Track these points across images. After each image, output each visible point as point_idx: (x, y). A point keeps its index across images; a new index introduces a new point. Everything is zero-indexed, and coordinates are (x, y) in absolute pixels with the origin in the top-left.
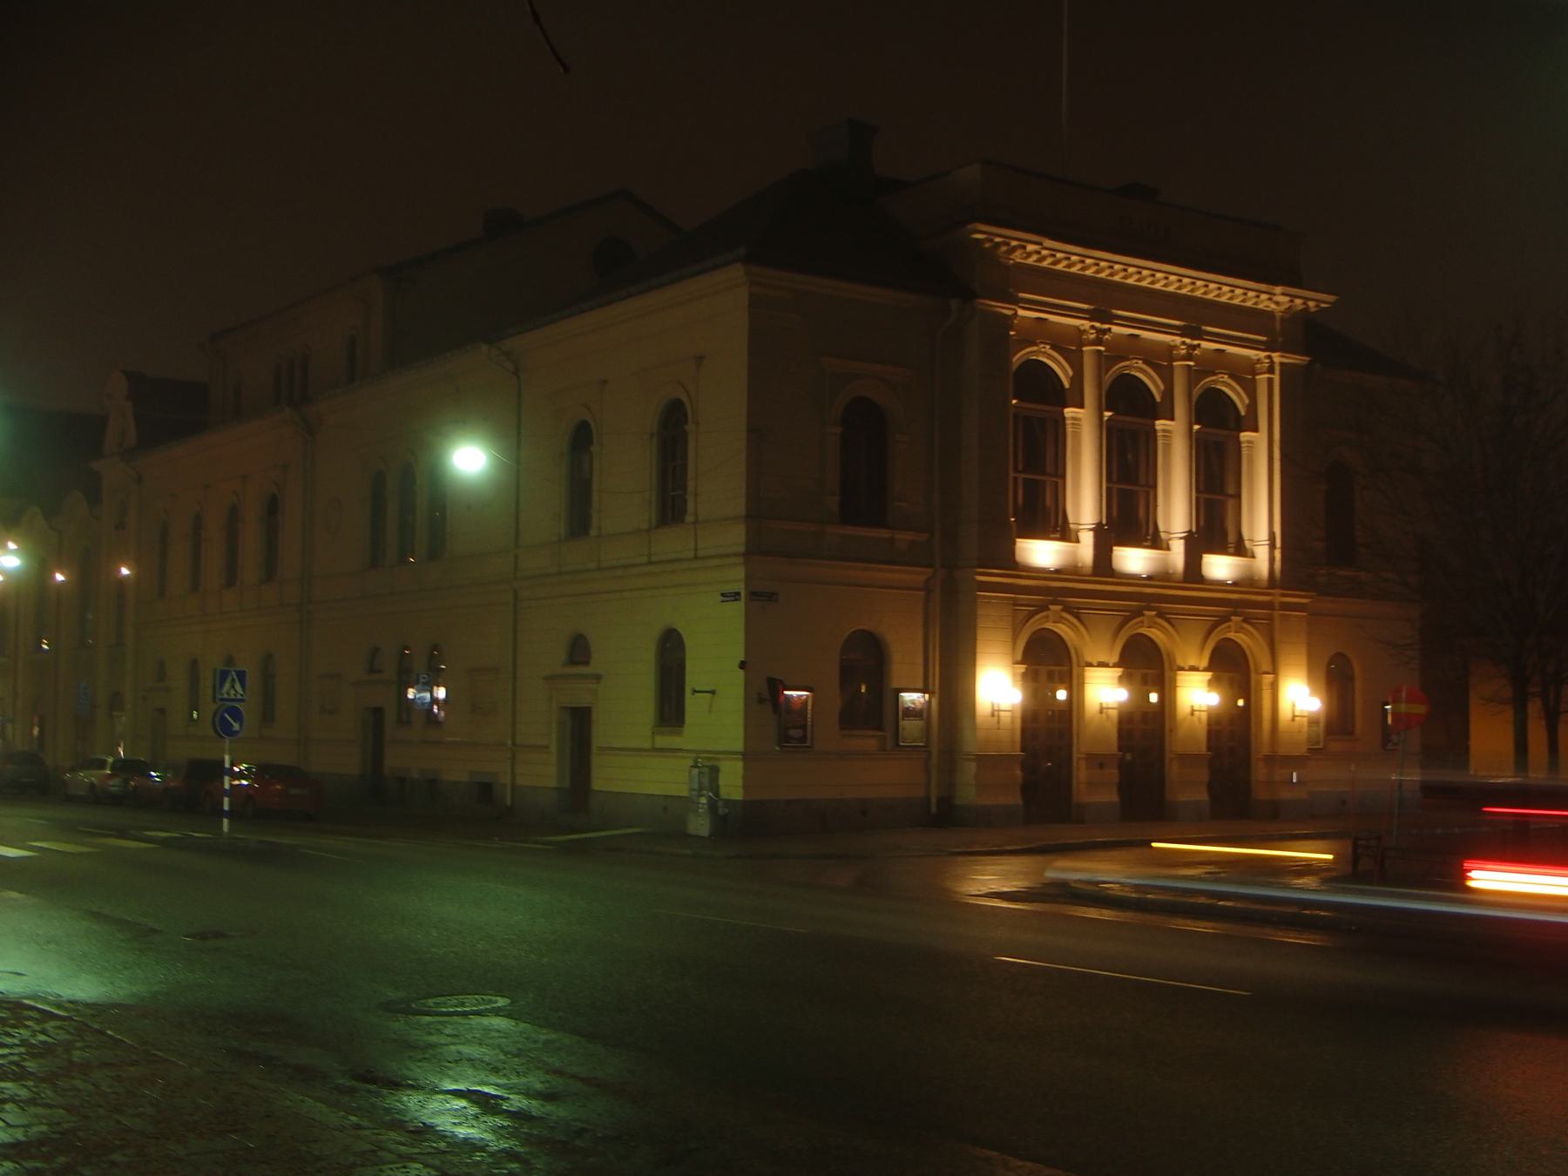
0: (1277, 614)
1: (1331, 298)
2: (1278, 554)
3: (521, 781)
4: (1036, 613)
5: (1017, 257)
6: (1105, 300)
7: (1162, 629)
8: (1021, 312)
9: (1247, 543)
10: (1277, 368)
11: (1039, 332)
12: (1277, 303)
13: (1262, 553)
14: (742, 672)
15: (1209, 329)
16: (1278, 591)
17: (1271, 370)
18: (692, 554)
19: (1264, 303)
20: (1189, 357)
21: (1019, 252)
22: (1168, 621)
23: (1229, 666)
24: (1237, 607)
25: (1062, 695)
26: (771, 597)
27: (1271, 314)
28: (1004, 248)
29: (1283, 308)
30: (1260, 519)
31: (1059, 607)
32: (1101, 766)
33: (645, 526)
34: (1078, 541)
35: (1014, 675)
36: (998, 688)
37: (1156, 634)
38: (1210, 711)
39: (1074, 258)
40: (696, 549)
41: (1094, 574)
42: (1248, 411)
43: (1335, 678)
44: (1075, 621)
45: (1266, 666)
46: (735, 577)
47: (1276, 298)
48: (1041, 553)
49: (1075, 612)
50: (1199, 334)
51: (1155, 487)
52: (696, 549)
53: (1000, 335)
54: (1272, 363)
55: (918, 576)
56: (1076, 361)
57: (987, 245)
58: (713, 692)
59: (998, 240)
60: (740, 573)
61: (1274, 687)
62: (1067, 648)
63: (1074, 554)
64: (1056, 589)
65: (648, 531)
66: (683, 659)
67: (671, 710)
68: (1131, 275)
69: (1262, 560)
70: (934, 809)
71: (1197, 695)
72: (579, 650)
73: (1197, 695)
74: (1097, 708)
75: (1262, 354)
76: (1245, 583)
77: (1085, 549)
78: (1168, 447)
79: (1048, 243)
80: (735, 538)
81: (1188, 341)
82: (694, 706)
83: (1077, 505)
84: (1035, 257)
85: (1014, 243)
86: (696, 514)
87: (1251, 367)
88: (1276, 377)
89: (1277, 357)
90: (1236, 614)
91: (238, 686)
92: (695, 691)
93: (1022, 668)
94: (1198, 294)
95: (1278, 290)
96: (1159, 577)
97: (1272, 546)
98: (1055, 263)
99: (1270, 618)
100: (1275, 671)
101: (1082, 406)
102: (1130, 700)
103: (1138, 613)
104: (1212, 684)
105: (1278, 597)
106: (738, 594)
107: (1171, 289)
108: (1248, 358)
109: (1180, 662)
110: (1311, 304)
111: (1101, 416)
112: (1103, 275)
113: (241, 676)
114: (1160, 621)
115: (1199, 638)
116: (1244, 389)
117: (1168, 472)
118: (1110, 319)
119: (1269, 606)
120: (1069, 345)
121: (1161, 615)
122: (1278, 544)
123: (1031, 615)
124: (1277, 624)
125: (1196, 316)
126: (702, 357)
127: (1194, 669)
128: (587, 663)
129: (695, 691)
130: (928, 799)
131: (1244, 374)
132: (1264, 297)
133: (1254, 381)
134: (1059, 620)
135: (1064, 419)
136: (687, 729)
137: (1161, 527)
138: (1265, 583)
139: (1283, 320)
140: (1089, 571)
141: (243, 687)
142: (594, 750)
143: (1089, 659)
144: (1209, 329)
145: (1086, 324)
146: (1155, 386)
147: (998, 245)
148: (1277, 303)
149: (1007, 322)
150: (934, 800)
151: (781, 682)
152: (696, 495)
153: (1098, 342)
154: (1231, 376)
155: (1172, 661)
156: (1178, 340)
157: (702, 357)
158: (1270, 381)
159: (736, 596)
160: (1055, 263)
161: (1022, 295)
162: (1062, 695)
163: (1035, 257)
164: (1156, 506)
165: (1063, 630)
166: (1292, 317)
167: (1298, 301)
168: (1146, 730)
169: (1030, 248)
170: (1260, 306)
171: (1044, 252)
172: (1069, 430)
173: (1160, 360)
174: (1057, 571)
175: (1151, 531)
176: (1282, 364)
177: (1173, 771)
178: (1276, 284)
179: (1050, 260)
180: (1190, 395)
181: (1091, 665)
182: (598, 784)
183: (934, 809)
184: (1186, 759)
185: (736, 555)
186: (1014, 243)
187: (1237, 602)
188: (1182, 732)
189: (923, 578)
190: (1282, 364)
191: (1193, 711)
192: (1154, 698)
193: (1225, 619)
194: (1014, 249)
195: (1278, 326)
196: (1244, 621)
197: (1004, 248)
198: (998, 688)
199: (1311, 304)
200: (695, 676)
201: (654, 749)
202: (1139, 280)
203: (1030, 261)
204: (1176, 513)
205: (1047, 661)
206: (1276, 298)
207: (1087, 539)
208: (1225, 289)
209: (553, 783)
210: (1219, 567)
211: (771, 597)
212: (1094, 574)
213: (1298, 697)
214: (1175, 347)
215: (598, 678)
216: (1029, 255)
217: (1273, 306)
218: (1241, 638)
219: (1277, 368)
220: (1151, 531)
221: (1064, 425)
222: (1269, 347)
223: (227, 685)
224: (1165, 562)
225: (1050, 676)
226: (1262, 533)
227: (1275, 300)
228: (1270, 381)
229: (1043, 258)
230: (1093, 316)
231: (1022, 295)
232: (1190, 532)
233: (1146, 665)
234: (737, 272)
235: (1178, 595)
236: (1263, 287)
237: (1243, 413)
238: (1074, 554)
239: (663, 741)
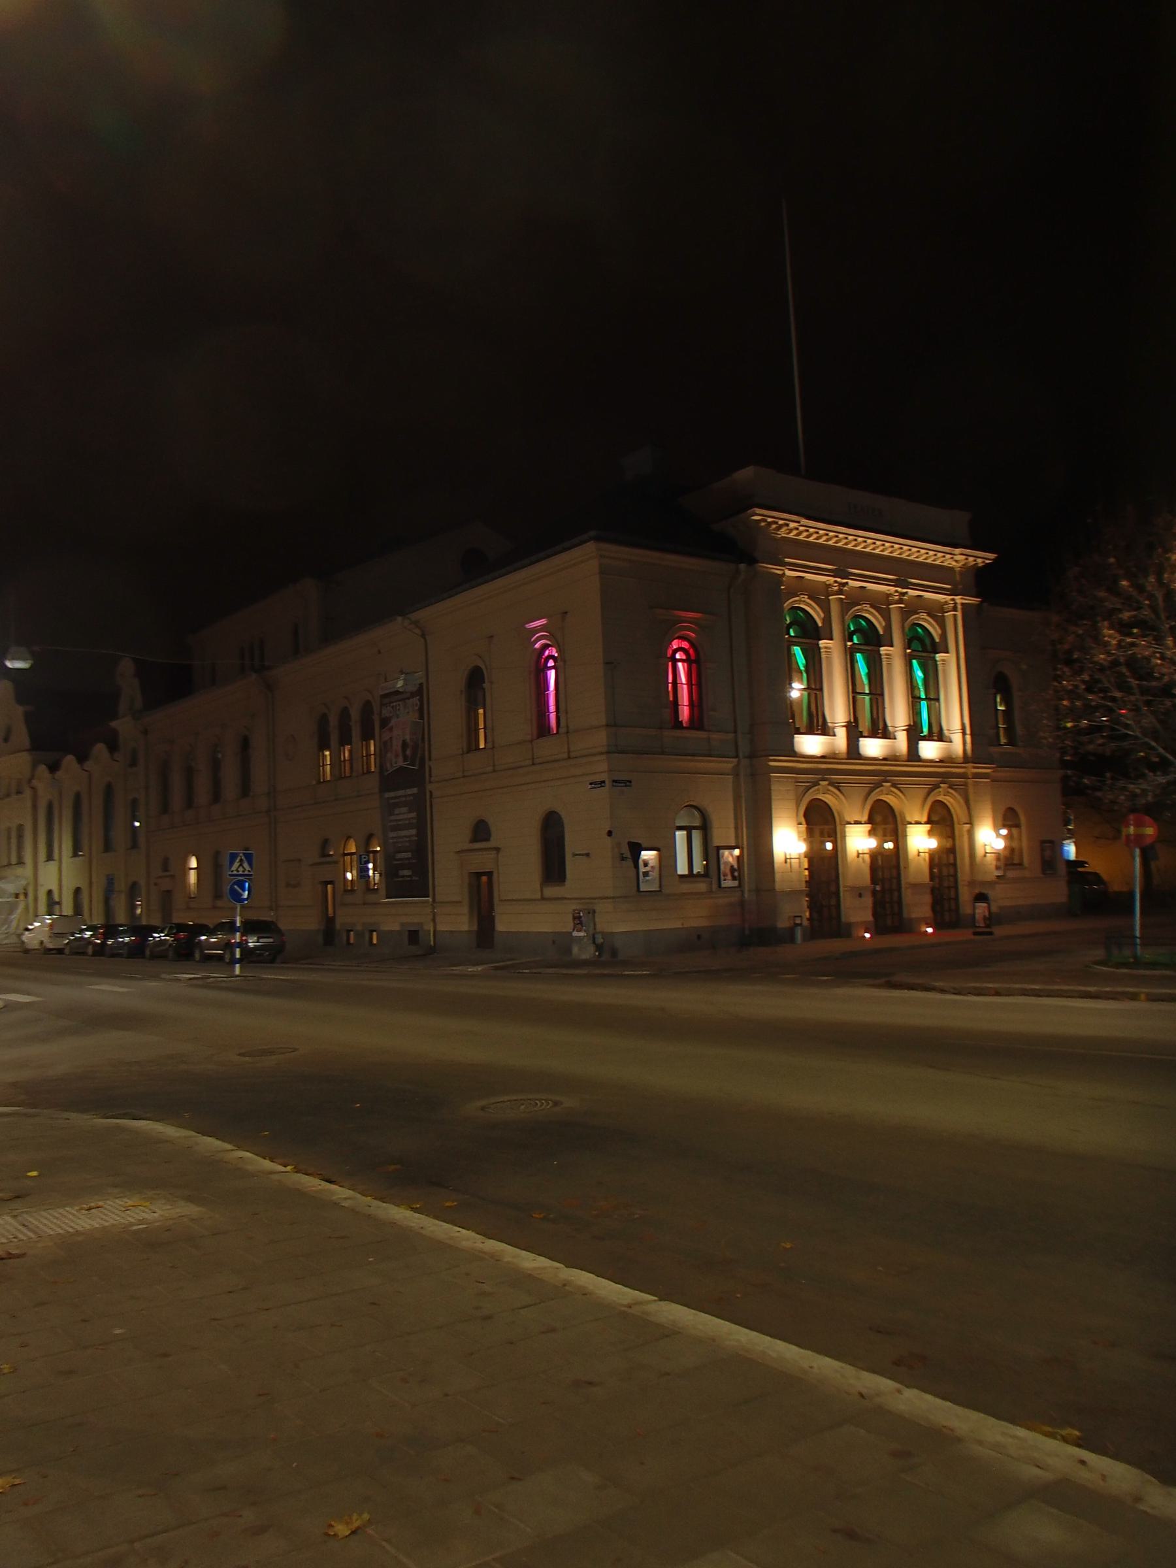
0: (970, 781)
1: (993, 556)
2: (968, 738)
3: (440, 928)
4: (811, 788)
5: (783, 533)
7: (896, 796)
8: (788, 573)
9: (946, 732)
10: (959, 607)
11: (800, 587)
13: (957, 738)
14: (608, 841)
17: (955, 609)
19: (948, 562)
22: (899, 789)
23: (941, 820)
27: (951, 569)
28: (774, 526)
30: (954, 715)
32: (860, 895)
33: (529, 738)
35: (799, 832)
36: (788, 842)
40: (569, 752)
42: (824, 620)
45: (964, 819)
46: (601, 768)
48: (810, 745)
50: (907, 585)
51: (882, 695)
53: (776, 590)
55: (728, 765)
56: (826, 607)
58: (587, 855)
60: (604, 766)
63: (832, 744)
64: (823, 770)
67: (554, 867)
69: (958, 744)
70: (747, 932)
71: (920, 841)
72: (481, 831)
74: (783, 859)
76: (944, 761)
77: (840, 740)
79: (804, 521)
80: (601, 739)
83: (832, 708)
85: (781, 522)
88: (959, 614)
89: (958, 599)
91: (246, 865)
95: (957, 551)
97: (964, 733)
99: (966, 784)
100: (971, 823)
101: (892, 646)
103: (878, 785)
104: (930, 833)
105: (971, 769)
109: (909, 819)
113: (249, 858)
115: (919, 801)
116: (936, 621)
118: (847, 576)
120: (820, 595)
121: (894, 785)
122: (968, 731)
124: (971, 790)
125: (904, 572)
128: (487, 840)
131: (937, 613)
132: (948, 556)
134: (826, 792)
136: (568, 882)
137: (889, 723)
139: (961, 573)
140: (905, 758)
141: (250, 864)
146: (817, 615)
147: (770, 524)
151: (639, 845)
153: (840, 592)
154: (929, 614)
155: (903, 818)
156: (832, 579)
160: (827, 540)
163: (795, 532)
164: (884, 708)
165: (828, 799)
167: (971, 559)
168: (887, 867)
169: (792, 525)
171: (801, 528)
172: (823, 656)
173: (881, 604)
175: (881, 726)
176: (962, 604)
177: (908, 896)
179: (825, 538)
180: (903, 628)
182: (500, 927)
183: (747, 932)
184: (915, 886)
186: (781, 522)
187: (943, 774)
188: (912, 868)
189: (730, 765)
192: (829, 846)
194: (780, 527)
195: (958, 577)
197: (774, 526)
198: (788, 842)
199: (979, 560)
200: (572, 843)
201: (543, 899)
204: (898, 715)
205: (821, 822)
206: (957, 558)
207: (841, 733)
209: (465, 928)
210: (929, 750)
213: (989, 838)
214: (890, 595)
215: (497, 849)
216: (791, 531)
218: (947, 800)
219: (959, 607)
220: (881, 726)
221: (881, 659)
223: (236, 864)
224: (832, 744)
225: (822, 835)
226: (956, 725)
227: (956, 558)
230: (897, 584)
233: (886, 822)
234: (590, 547)
235: (903, 770)
237: (881, 632)
239: (550, 891)
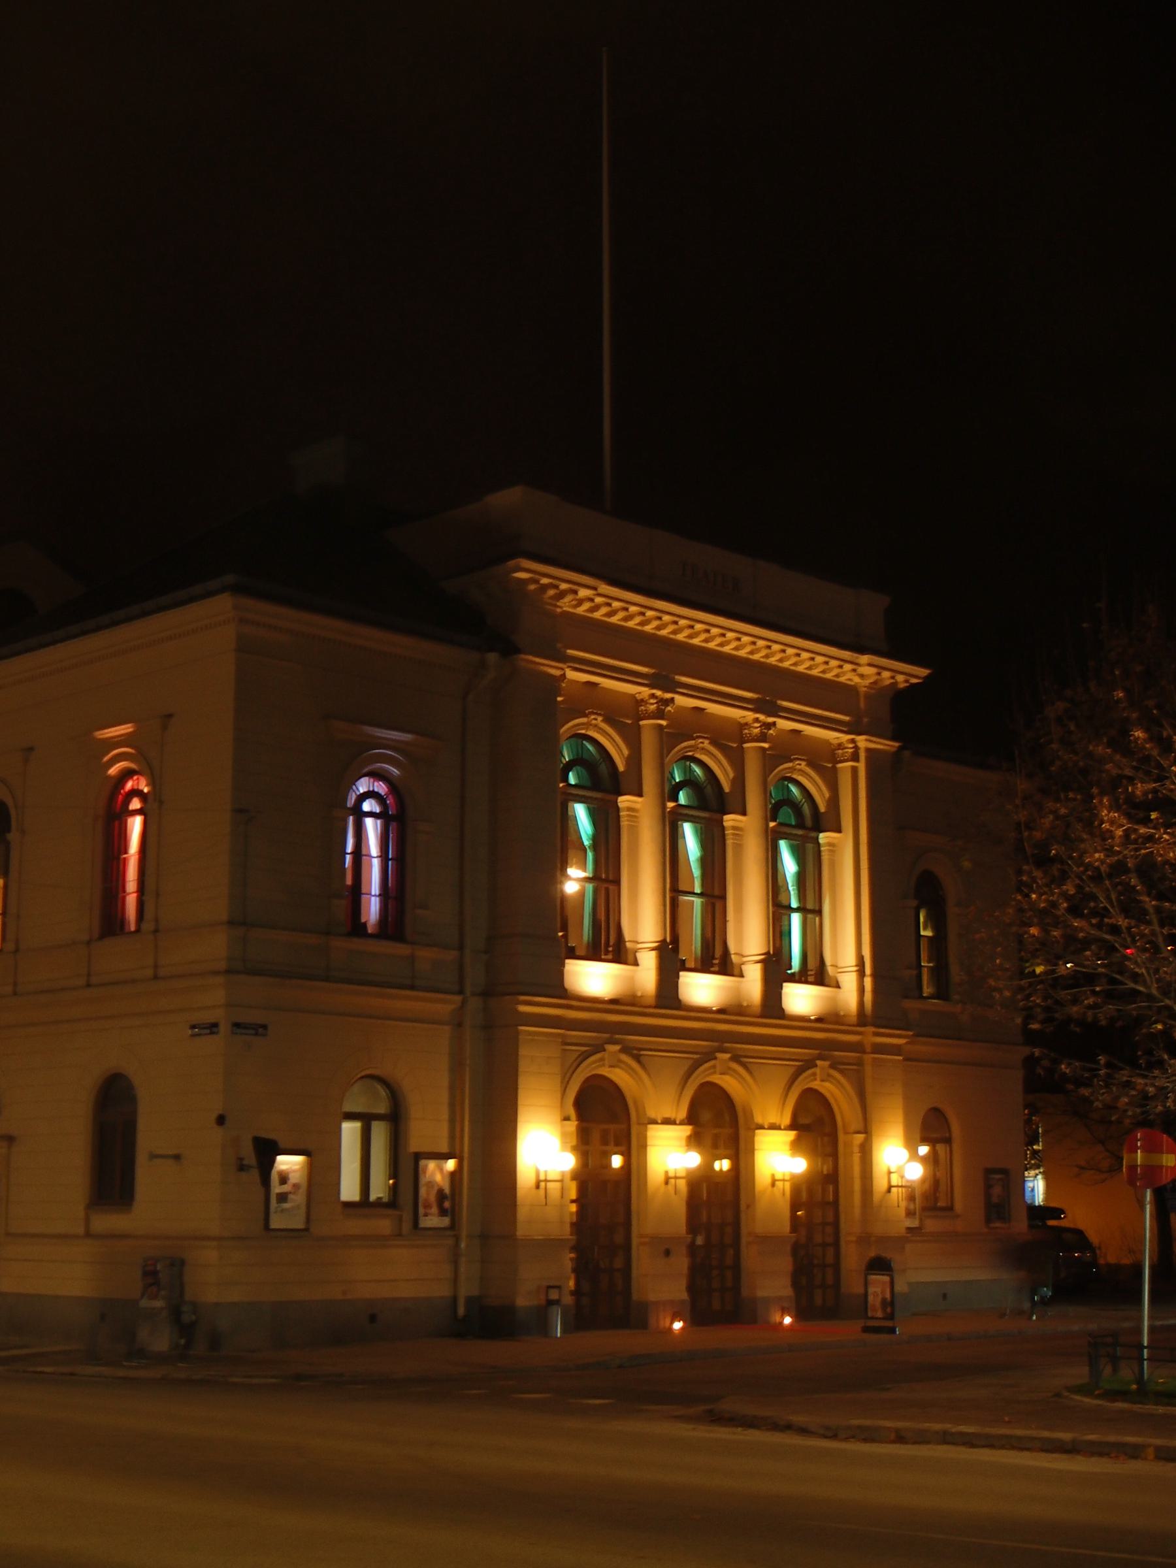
0: (868, 1058)
2: (868, 982)
5: (566, 605)
6: (668, 662)
8: (572, 675)
9: (830, 970)
10: (862, 755)
11: (590, 701)
12: (862, 676)
13: (849, 981)
15: (684, 679)
16: (872, 1029)
17: (855, 757)
18: (150, 972)
19: (848, 676)
23: (814, 1126)
24: (825, 1048)
25: (617, 1161)
26: (260, 1029)
27: (851, 690)
28: (551, 592)
29: (867, 682)
30: (847, 942)
32: (667, 1253)
33: (222, 965)
35: (564, 1135)
36: (544, 1151)
38: (794, 1178)
39: (633, 609)
40: (156, 966)
44: (634, 1064)
45: (855, 1122)
47: (861, 670)
48: (593, 978)
49: (635, 1053)
50: (774, 711)
54: (856, 748)
55: (445, 1006)
57: (532, 587)
58: (177, 1157)
64: (613, 1022)
65: (89, 943)
69: (849, 992)
70: (461, 1311)
73: (778, 1160)
74: (662, 1178)
75: (845, 738)
76: (828, 1019)
79: (605, 588)
82: (148, 1178)
84: (586, 606)
85: (564, 586)
86: (157, 920)
87: (739, 731)
88: (862, 766)
89: (862, 741)
90: (821, 1057)
92: (153, 1156)
93: (572, 1126)
94: (772, 660)
95: (864, 659)
96: (731, 1011)
97: (861, 973)
98: (626, 619)
99: (860, 1063)
100: (866, 1130)
103: (709, 1056)
104: (797, 1146)
105: (870, 1036)
106: (215, 1025)
108: (827, 742)
109: (759, 1119)
110: (900, 678)
111: (664, 807)
112: (664, 632)
114: (734, 1066)
117: (739, 883)
118: (672, 686)
119: (858, 1048)
120: (626, 718)
121: (736, 1058)
122: (868, 970)
123: (585, 1056)
124: (868, 1070)
125: (771, 687)
127: (774, 1127)
129: (153, 1156)
130: (455, 1299)
131: (824, 761)
132: (848, 667)
133: (834, 770)
135: (618, 809)
138: (854, 1020)
139: (868, 697)
140: (652, 1001)
143: (651, 1113)
144: (684, 679)
145: (645, 692)
148: (862, 676)
152: (158, 895)
155: (749, 1115)
159: (213, 1027)
160: (626, 619)
161: (570, 652)
162: (617, 1161)
163: (586, 606)
164: (725, 922)
165: (619, 1076)
166: (877, 692)
167: (886, 674)
168: (718, 1203)
169: (583, 593)
170: (842, 679)
171: (598, 600)
172: (624, 823)
174: (613, 1001)
176: (868, 750)
177: (751, 1257)
181: (655, 1122)
183: (461, 1311)
184: (766, 1241)
186: (564, 586)
187: (823, 1041)
188: (762, 1205)
189: (450, 1007)
191: (774, 1182)
193: (809, 1064)
194: (562, 595)
195: (862, 704)
196: (832, 1066)
198: (544, 1151)
199: (900, 678)
200: (151, 1134)
202: (706, 641)
203: (581, 610)
205: (602, 1119)
206: (861, 670)
207: (648, 962)
211: (260, 1029)
213: (897, 1161)
214: (642, 702)
216: (580, 602)
217: (857, 680)
218: (827, 1088)
219: (862, 755)
221: (618, 817)
224: (737, 991)
227: (861, 671)
228: (855, 770)
229: (596, 608)
230: (654, 682)
231: (570, 652)
233: (719, 1123)
234: (223, 605)
236: (846, 654)
238: (631, 979)
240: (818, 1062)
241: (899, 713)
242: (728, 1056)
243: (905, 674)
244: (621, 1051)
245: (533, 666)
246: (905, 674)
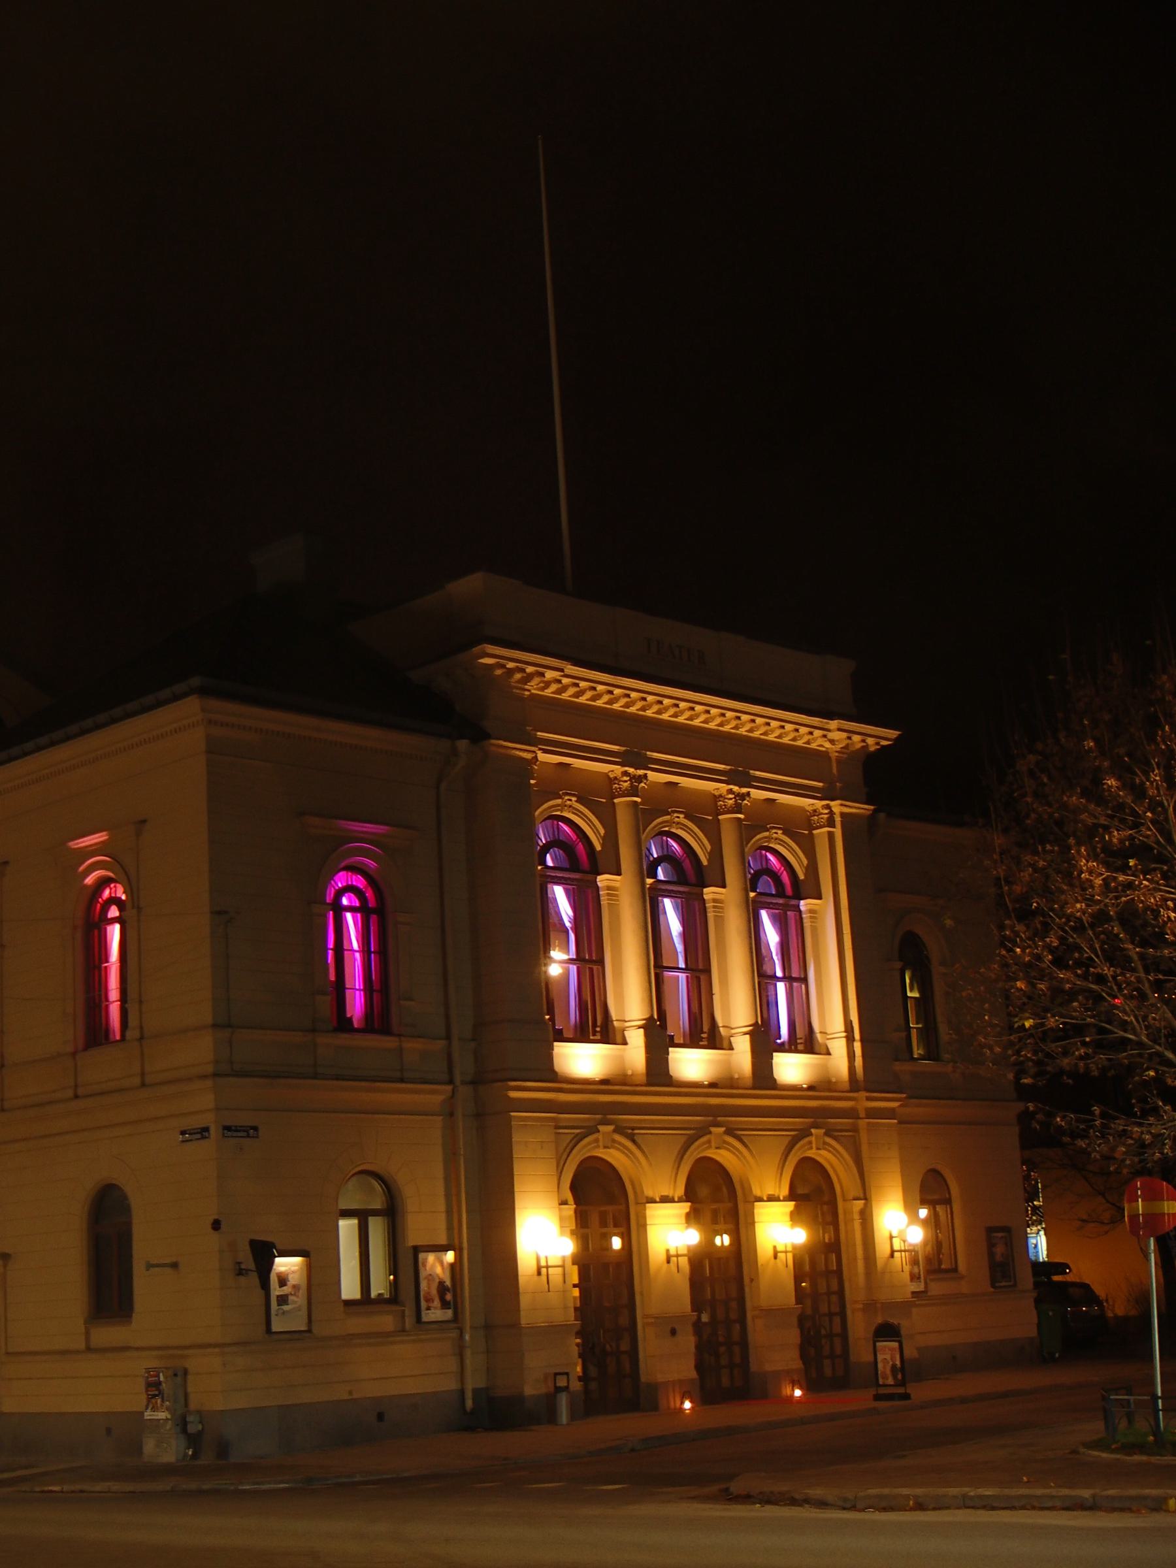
0: (862, 1123)
1: (893, 734)
2: (857, 1046)
5: (533, 687)
6: (638, 739)
8: (542, 757)
9: (819, 1036)
10: (838, 819)
11: (564, 782)
12: (832, 742)
13: (839, 1047)
15: (758, 773)
16: (863, 1094)
17: (831, 823)
19: (818, 742)
20: (737, 809)
21: (536, 680)
23: (812, 1195)
24: (818, 1116)
27: (823, 756)
28: (518, 676)
29: (839, 747)
30: (833, 1008)
31: (611, 1128)
34: (625, 1043)
35: (562, 1219)
36: (543, 1236)
37: (724, 1157)
40: (143, 1074)
41: (649, 1084)
43: (929, 1191)
44: (629, 1144)
45: (853, 1189)
47: (831, 735)
48: (582, 1060)
50: (747, 781)
52: (143, 1074)
54: (831, 813)
55: (434, 1097)
57: (499, 672)
58: (175, 1265)
59: (511, 665)
60: (207, 1100)
61: (867, 1219)
62: (620, 1178)
64: (605, 1103)
65: (74, 1054)
66: (129, 1225)
68: (666, 709)
69: (839, 1057)
70: (469, 1404)
74: (663, 1257)
75: (819, 804)
76: (820, 1087)
77: (635, 1051)
78: (720, 920)
80: (201, 1051)
81: (735, 788)
82: (146, 1288)
83: (620, 997)
84: (554, 687)
85: (530, 669)
88: (838, 831)
89: (836, 806)
90: (817, 1127)
92: (149, 1266)
93: (569, 1210)
94: (743, 731)
95: (834, 724)
96: (722, 1084)
97: (850, 1039)
99: (855, 1129)
100: (866, 1197)
102: (700, 1242)
103: (703, 1131)
104: (795, 1217)
105: (863, 1101)
106: (206, 1129)
107: (712, 725)
109: (757, 1192)
110: (870, 741)
112: (633, 709)
115: (777, 1159)
118: (644, 763)
119: (852, 1114)
120: (600, 798)
121: (730, 1132)
123: (579, 1138)
124: (864, 1137)
125: (742, 758)
126: (144, 822)
129: (149, 1266)
130: (462, 1392)
131: (800, 829)
132: (817, 733)
137: (720, 1022)
139: (839, 761)
142: (138, 1268)
143: (649, 1193)
144: (758, 773)
145: (617, 770)
147: (511, 672)
148: (832, 742)
149: (525, 768)
150: (469, 1395)
151: (271, 1245)
155: (747, 1189)
156: (723, 787)
157: (144, 822)
158: (831, 836)
159: (204, 1132)
162: (617, 1243)
164: (711, 994)
168: (721, 1278)
169: (550, 675)
170: (813, 746)
171: (565, 681)
173: (705, 813)
174: (604, 1082)
176: (842, 815)
178: (830, 716)
183: (469, 1404)
184: (769, 1313)
185: (204, 1077)
186: (530, 669)
187: (816, 1109)
190: (842, 815)
194: (529, 677)
196: (827, 1134)
197: (518, 676)
198: (543, 1236)
200: (147, 1243)
203: (548, 692)
205: (600, 1200)
206: (831, 735)
207: (636, 1039)
208: (789, 727)
212: (649, 1084)
213: (898, 1225)
216: (547, 684)
217: (828, 745)
218: (823, 1157)
219: (838, 819)
222: (828, 795)
226: (836, 1024)
227: (831, 737)
228: (831, 836)
229: (564, 689)
230: (628, 759)
232: (755, 1025)
233: (718, 1198)
234: (191, 707)
236: (815, 721)
238: (621, 1059)
239: (107, 1334)
240: (813, 1131)
241: (872, 777)
242: (723, 1129)
243: (876, 737)
244: (615, 1131)
245: (503, 751)
246: (876, 737)
